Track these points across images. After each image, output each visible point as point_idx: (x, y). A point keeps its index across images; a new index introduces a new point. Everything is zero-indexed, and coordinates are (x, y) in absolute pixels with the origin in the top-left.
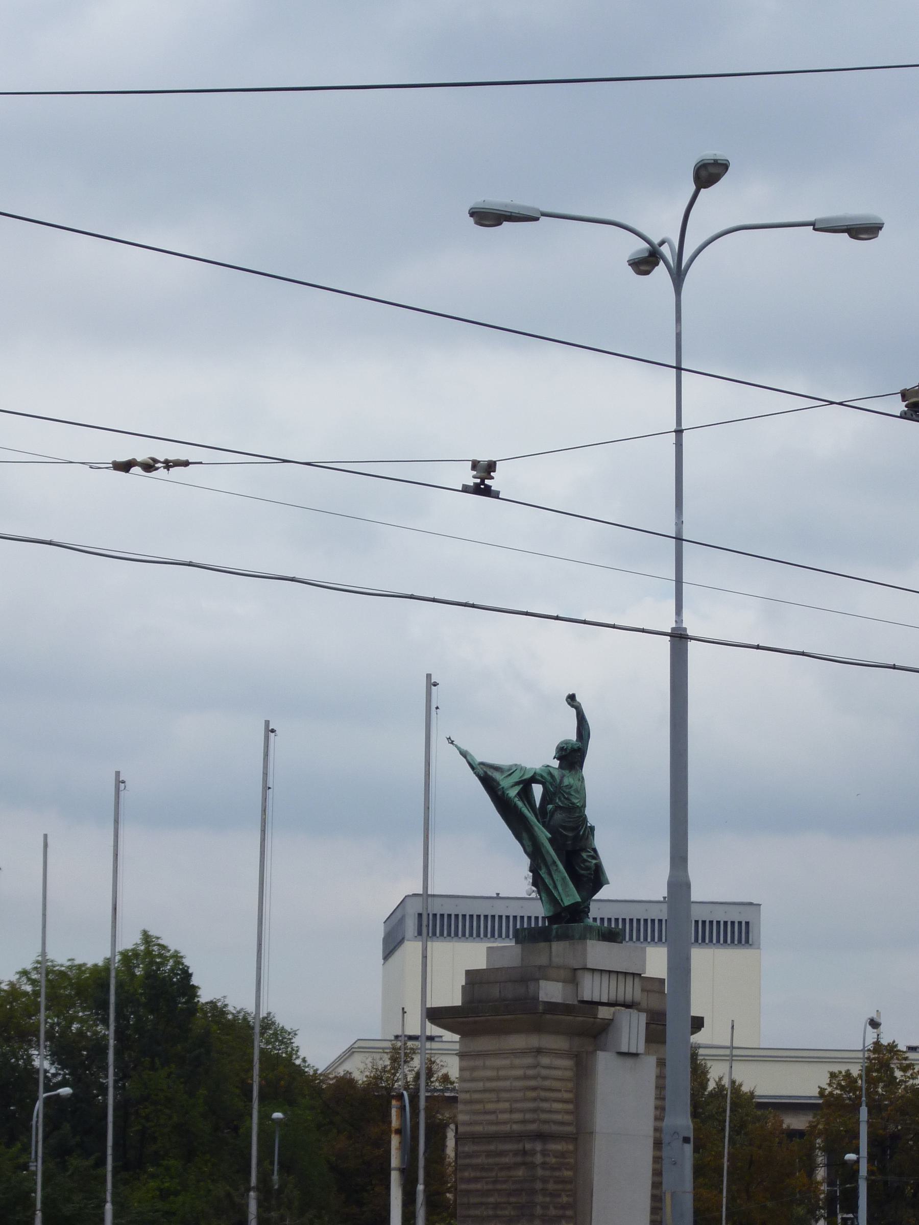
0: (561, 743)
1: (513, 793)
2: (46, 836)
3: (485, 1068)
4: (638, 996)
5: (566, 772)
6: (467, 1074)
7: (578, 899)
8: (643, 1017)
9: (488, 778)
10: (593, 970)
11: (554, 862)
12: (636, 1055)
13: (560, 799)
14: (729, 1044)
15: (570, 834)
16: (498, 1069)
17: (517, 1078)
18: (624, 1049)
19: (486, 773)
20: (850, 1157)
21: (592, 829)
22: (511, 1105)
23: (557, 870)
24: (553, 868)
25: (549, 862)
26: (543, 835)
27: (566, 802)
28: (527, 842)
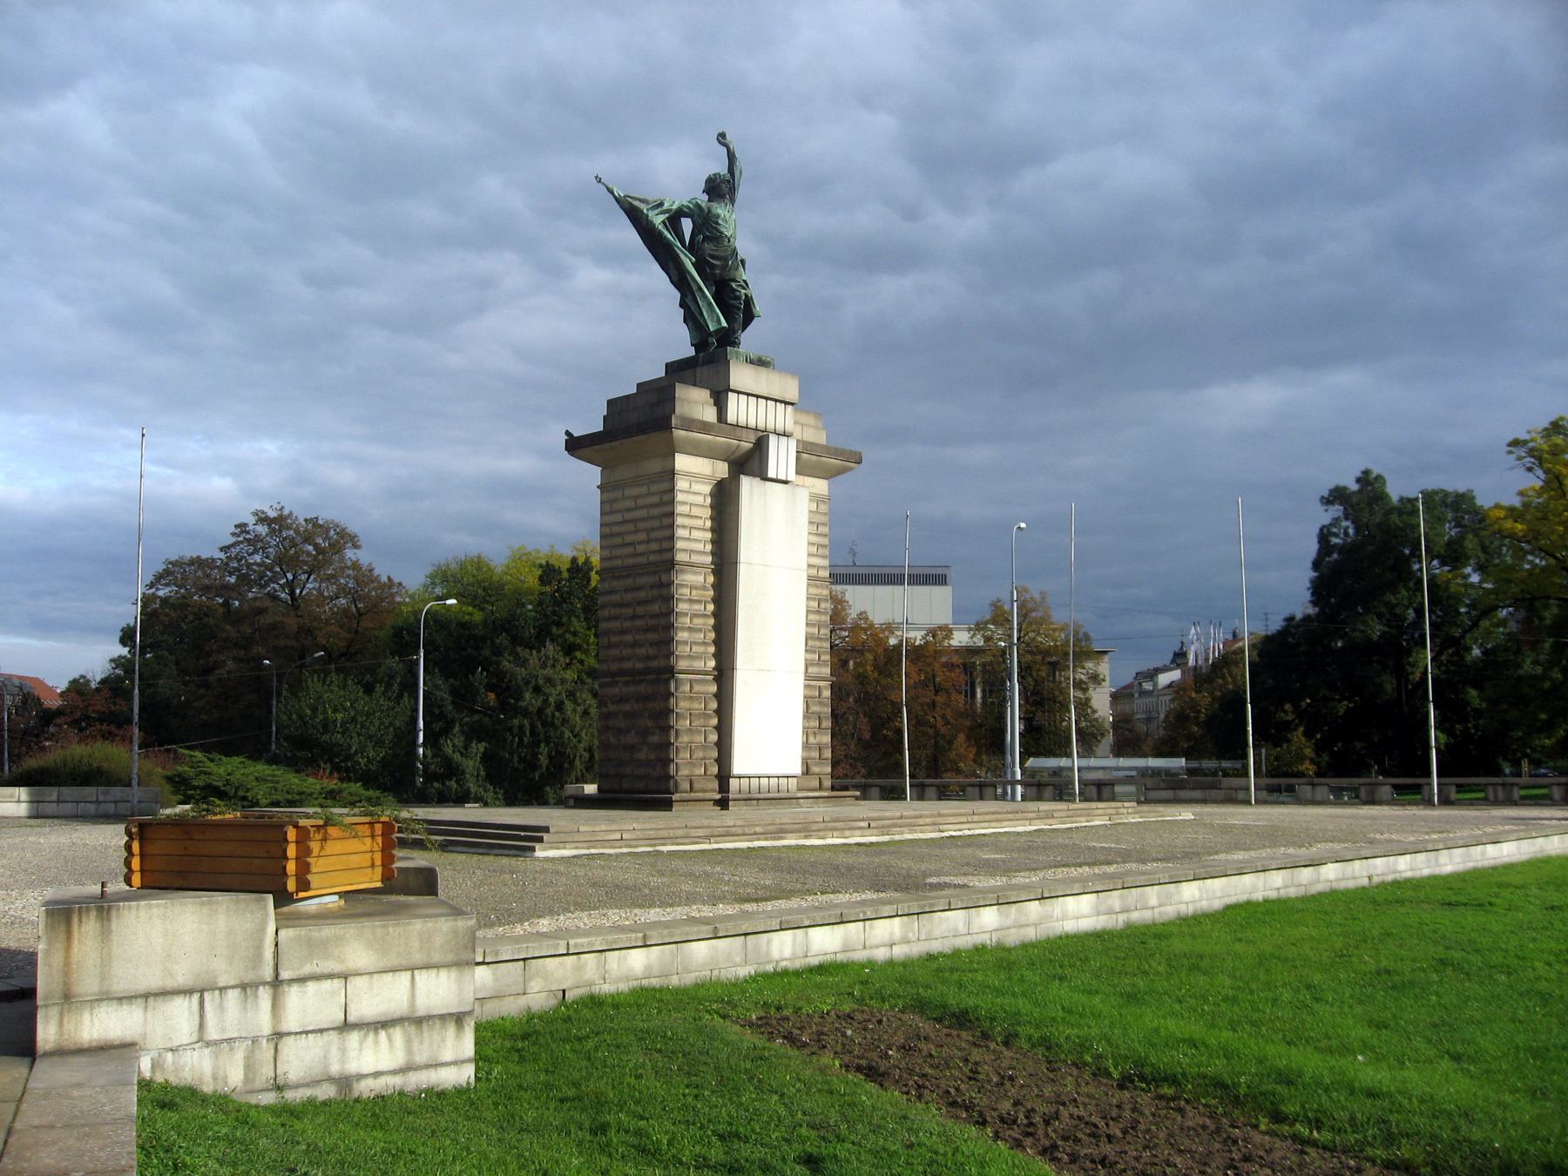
3: (624, 498)
6: (607, 508)
11: (700, 289)
14: (285, 974)
16: (636, 498)
17: (653, 506)
20: (1416, 567)
22: (1155, 685)
26: (688, 262)
28: (672, 272)
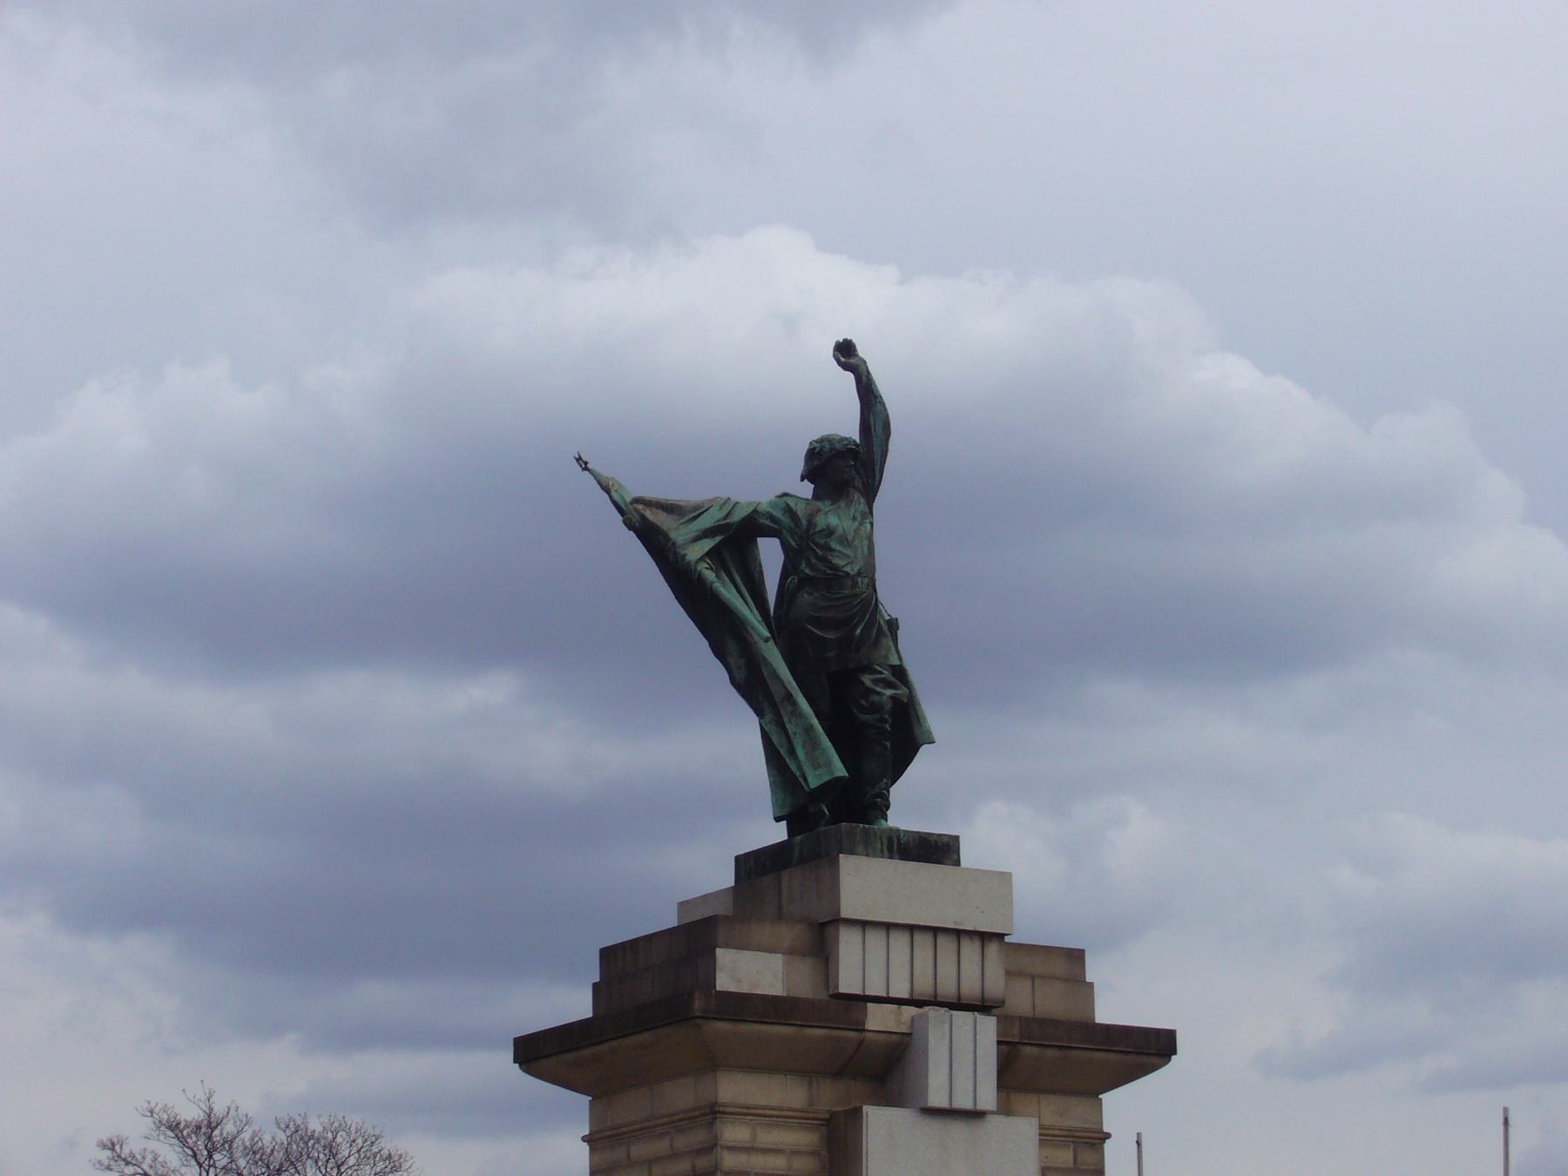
0: (821, 441)
1: (695, 552)
2: (1506, 1110)
4: (996, 984)
5: (824, 506)
7: (840, 771)
8: (988, 1027)
9: (648, 526)
10: (864, 925)
11: (789, 697)
12: (976, 1115)
13: (809, 564)
15: (831, 636)
18: (937, 1099)
19: (643, 517)
21: (893, 625)
23: (796, 713)
24: (785, 710)
25: (778, 695)
27: (820, 566)
